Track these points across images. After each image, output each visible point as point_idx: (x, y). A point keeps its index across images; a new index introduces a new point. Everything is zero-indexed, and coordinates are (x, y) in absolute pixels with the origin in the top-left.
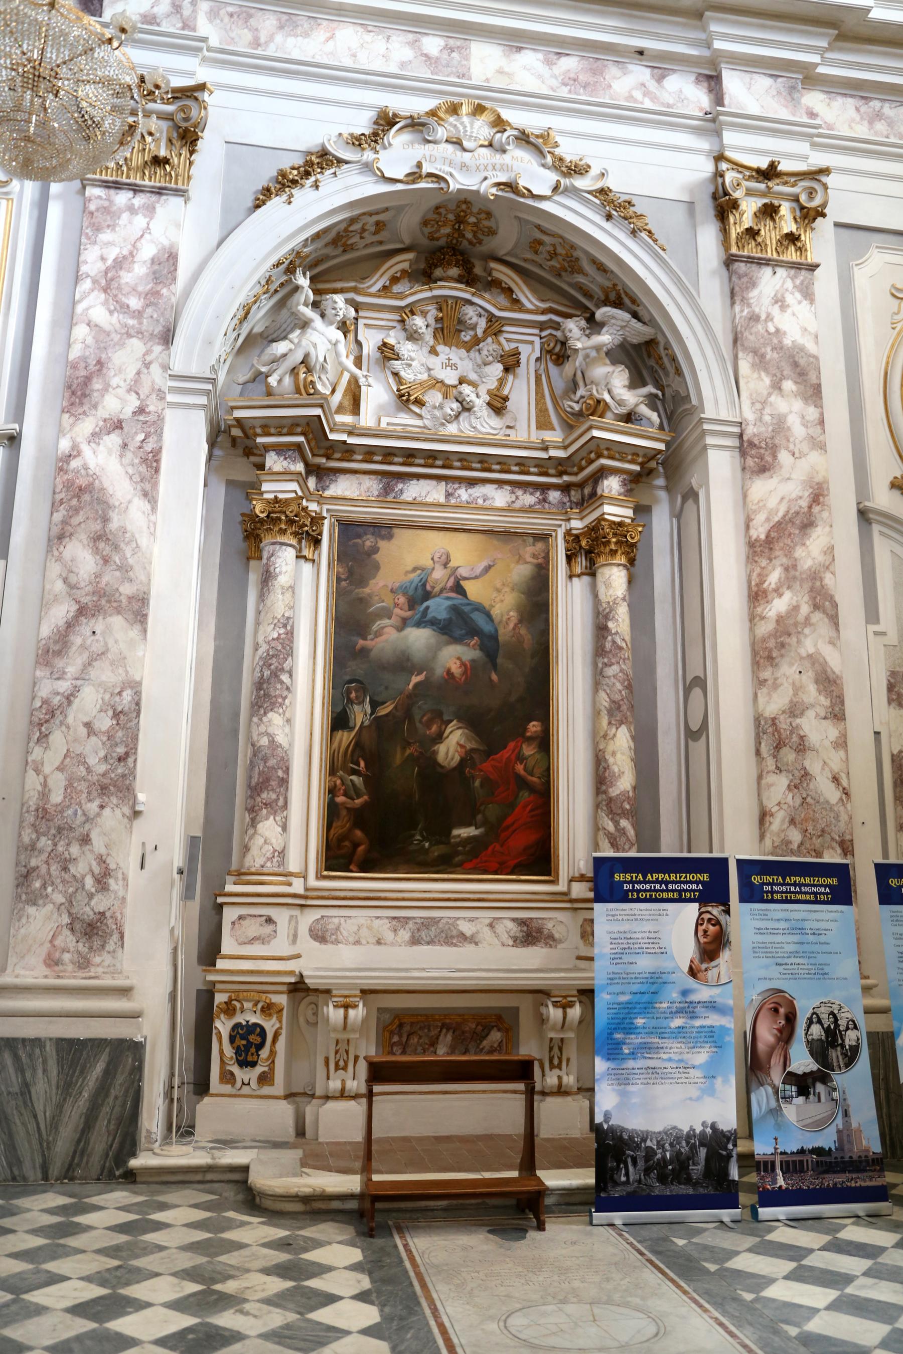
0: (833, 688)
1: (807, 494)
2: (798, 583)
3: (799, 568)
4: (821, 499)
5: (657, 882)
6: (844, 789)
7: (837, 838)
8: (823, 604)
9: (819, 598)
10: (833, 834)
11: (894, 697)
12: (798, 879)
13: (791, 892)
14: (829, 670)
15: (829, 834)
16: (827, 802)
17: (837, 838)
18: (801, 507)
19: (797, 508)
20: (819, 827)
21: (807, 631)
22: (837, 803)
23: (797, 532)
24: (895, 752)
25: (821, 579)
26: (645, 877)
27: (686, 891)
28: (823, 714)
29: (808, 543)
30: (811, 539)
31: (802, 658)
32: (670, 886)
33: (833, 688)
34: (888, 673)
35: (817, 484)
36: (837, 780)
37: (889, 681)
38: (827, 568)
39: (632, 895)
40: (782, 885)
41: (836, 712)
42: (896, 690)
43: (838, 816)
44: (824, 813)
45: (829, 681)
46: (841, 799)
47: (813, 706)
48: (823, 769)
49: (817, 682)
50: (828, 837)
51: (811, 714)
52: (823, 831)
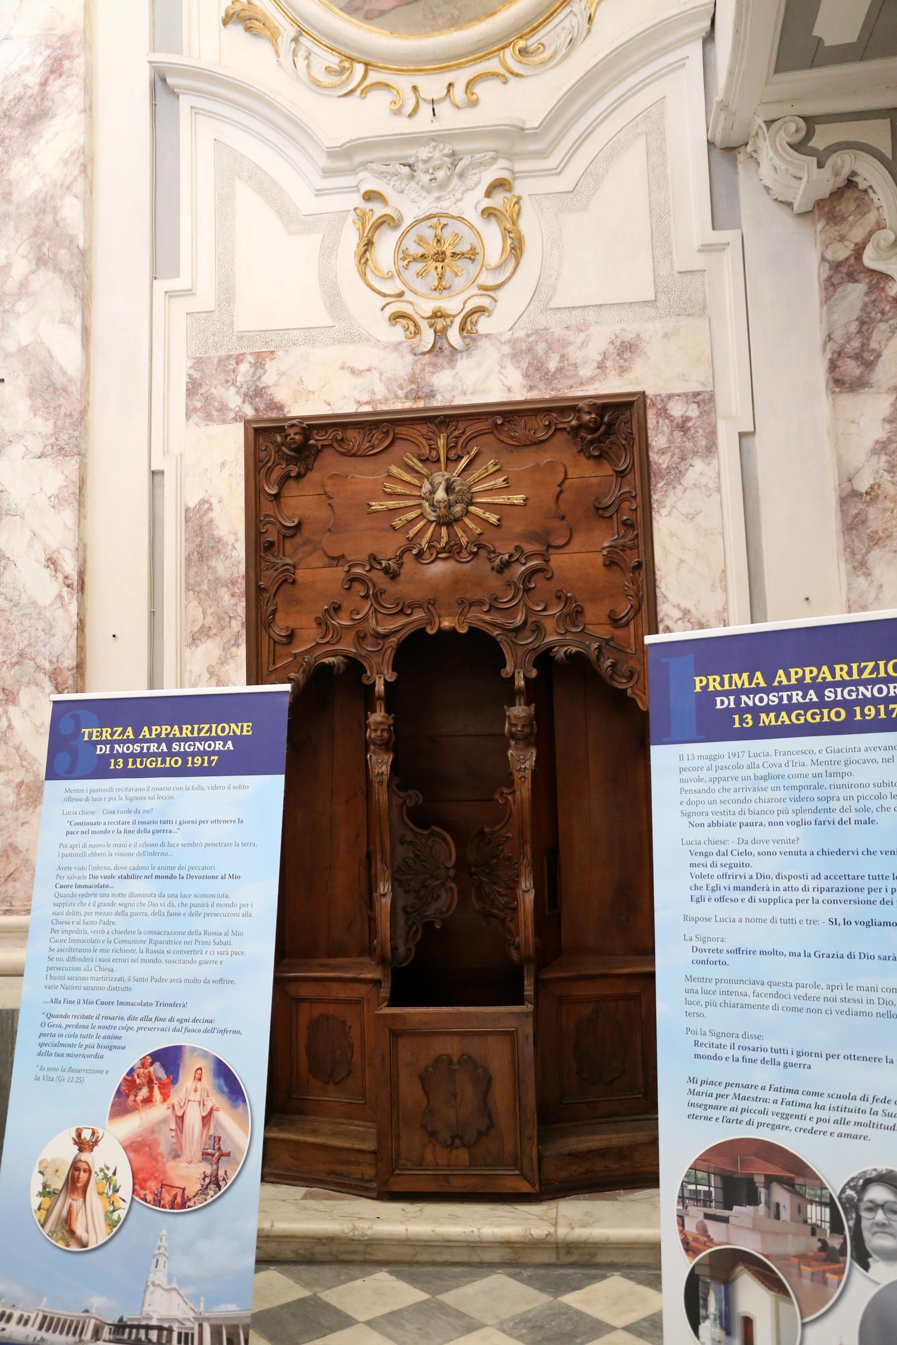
0: (62, 401)
1: (39, 60)
2: (12, 223)
3: (15, 197)
4: (66, 64)
5: (801, 685)
6: (66, 578)
7: (47, 666)
8: (55, 254)
9: (47, 244)
10: (41, 661)
11: (198, 405)
12: (165, 730)
13: (149, 755)
14: (55, 370)
15: (33, 659)
16: (34, 603)
17: (47, 666)
18: (26, 87)
19: (19, 90)
20: (15, 648)
21: (21, 307)
22: (52, 604)
23: (16, 132)
24: (192, 505)
25: (55, 210)
26: (769, 677)
27: (864, 702)
28: (38, 450)
29: (35, 149)
30: (42, 142)
31: (8, 355)
32: (829, 694)
33: (62, 401)
34: (191, 363)
35: (61, 38)
36: (54, 563)
37: (190, 376)
38: (68, 188)
39: (116, 764)
40: (768, 691)
41: (62, 443)
42: (202, 391)
43: (51, 626)
44: (27, 623)
45: (55, 389)
46: (60, 597)
47: (20, 437)
48: (30, 546)
49: (32, 393)
50: (29, 665)
51: (16, 451)
52: (21, 655)
